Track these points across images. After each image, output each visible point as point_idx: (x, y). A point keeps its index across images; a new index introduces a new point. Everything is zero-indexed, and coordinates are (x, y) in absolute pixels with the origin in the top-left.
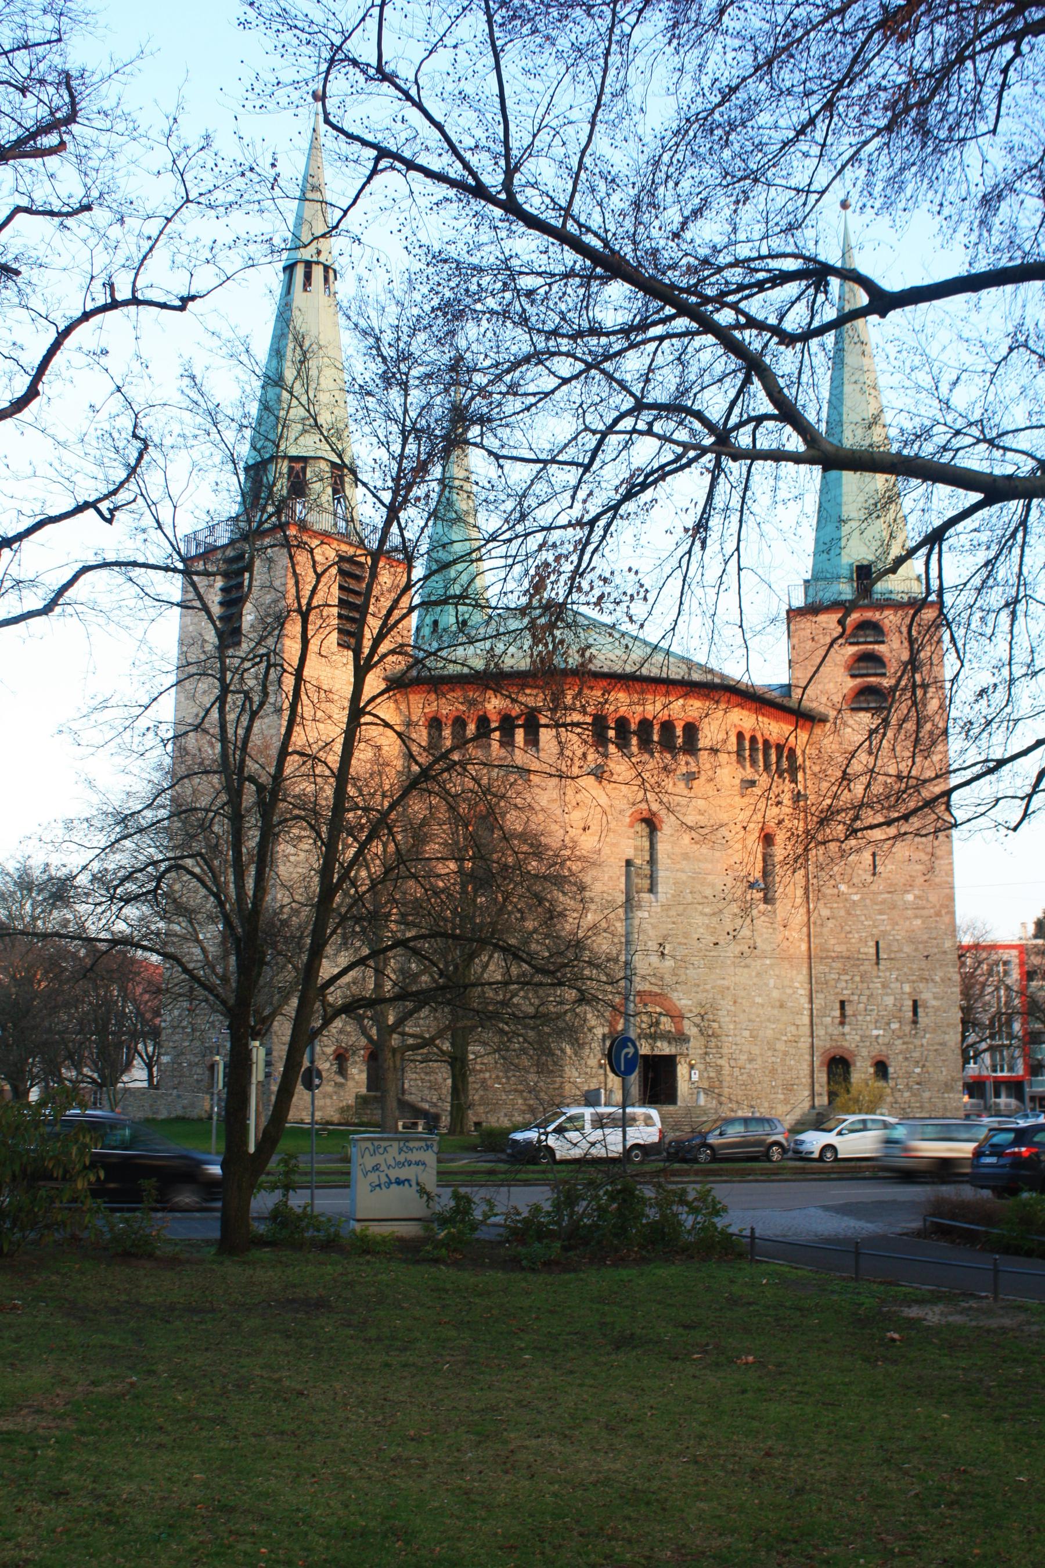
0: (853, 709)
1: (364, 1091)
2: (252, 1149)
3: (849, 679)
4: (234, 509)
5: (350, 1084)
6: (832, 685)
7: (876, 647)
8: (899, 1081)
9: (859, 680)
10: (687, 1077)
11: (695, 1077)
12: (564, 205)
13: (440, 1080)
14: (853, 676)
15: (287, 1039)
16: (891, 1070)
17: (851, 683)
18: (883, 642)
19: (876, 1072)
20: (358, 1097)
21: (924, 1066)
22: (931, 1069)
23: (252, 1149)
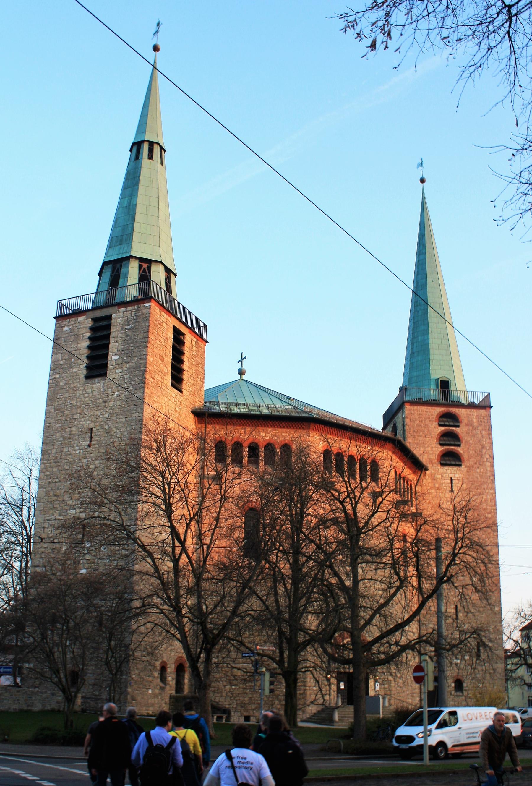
0: (442, 465)
1: (173, 692)
2: (127, 771)
3: (439, 446)
4: (38, 476)
5: (168, 687)
6: (429, 449)
7: (454, 428)
8: (470, 692)
9: (445, 447)
10: (373, 688)
11: (378, 688)
12: (429, 3)
13: (221, 686)
14: (441, 445)
15: (370, 689)
16: (465, 685)
17: (441, 449)
18: (458, 426)
19: (455, 687)
20: (171, 697)
21: (483, 683)
22: (487, 685)
23: (127, 771)
